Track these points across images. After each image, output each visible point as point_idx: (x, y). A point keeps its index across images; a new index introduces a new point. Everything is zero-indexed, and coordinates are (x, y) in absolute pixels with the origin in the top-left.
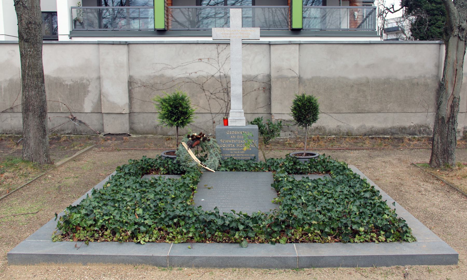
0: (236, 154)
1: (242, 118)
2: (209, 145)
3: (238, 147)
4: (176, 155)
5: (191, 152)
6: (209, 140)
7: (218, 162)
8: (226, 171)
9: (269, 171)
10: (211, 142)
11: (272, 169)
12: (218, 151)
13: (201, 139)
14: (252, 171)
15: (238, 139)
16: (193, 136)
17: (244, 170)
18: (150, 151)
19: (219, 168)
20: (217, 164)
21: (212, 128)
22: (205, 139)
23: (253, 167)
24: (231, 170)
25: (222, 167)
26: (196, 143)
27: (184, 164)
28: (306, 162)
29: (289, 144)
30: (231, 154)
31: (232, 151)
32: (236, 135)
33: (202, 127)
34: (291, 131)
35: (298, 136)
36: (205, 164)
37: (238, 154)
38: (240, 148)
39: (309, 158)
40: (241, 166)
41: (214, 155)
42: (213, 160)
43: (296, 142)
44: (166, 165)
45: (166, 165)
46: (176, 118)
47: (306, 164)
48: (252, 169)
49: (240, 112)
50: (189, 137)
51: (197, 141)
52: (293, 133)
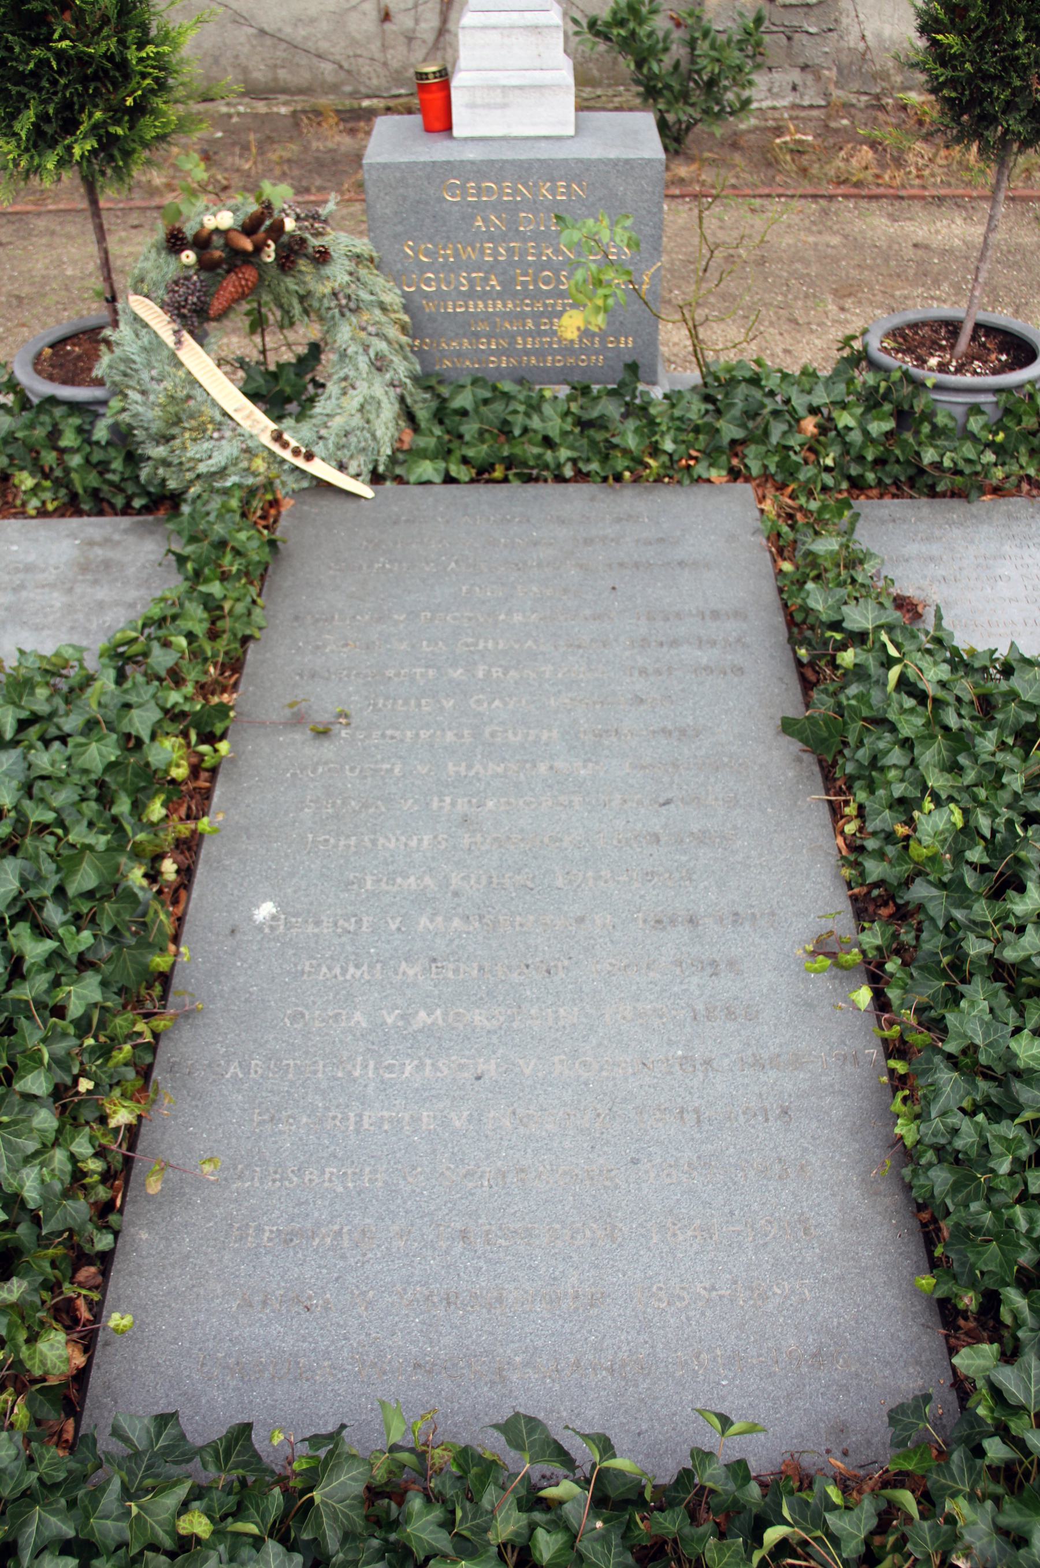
0: (512, 337)
1: (547, 77)
2: (326, 289)
3: (526, 294)
4: (99, 382)
5: (196, 359)
6: (323, 257)
7: (389, 410)
8: (449, 480)
9: (734, 475)
10: (338, 273)
11: (755, 471)
12: (393, 332)
13: (270, 254)
14: (618, 478)
15: (523, 238)
16: (202, 243)
17: (568, 472)
18: (41, 223)
19: (402, 456)
20: (386, 424)
21: (375, 47)
22: (292, 252)
23: (626, 452)
24: (482, 473)
25: (422, 454)
26: (231, 285)
27: (159, 451)
28: (975, 409)
29: (798, 151)
30: (477, 335)
31: (487, 317)
32: (513, 209)
33: (324, 46)
34: (804, 68)
35: (838, 94)
36: (306, 430)
37: (525, 334)
38: (537, 295)
39: (997, 391)
40: (548, 442)
41: (363, 362)
42: (362, 402)
43: (833, 140)
44: (49, 458)
45: (49, 458)
46: (44, 118)
47: (975, 424)
48: (620, 463)
49: (536, 29)
50: (175, 242)
51: (234, 275)
52: (810, 78)
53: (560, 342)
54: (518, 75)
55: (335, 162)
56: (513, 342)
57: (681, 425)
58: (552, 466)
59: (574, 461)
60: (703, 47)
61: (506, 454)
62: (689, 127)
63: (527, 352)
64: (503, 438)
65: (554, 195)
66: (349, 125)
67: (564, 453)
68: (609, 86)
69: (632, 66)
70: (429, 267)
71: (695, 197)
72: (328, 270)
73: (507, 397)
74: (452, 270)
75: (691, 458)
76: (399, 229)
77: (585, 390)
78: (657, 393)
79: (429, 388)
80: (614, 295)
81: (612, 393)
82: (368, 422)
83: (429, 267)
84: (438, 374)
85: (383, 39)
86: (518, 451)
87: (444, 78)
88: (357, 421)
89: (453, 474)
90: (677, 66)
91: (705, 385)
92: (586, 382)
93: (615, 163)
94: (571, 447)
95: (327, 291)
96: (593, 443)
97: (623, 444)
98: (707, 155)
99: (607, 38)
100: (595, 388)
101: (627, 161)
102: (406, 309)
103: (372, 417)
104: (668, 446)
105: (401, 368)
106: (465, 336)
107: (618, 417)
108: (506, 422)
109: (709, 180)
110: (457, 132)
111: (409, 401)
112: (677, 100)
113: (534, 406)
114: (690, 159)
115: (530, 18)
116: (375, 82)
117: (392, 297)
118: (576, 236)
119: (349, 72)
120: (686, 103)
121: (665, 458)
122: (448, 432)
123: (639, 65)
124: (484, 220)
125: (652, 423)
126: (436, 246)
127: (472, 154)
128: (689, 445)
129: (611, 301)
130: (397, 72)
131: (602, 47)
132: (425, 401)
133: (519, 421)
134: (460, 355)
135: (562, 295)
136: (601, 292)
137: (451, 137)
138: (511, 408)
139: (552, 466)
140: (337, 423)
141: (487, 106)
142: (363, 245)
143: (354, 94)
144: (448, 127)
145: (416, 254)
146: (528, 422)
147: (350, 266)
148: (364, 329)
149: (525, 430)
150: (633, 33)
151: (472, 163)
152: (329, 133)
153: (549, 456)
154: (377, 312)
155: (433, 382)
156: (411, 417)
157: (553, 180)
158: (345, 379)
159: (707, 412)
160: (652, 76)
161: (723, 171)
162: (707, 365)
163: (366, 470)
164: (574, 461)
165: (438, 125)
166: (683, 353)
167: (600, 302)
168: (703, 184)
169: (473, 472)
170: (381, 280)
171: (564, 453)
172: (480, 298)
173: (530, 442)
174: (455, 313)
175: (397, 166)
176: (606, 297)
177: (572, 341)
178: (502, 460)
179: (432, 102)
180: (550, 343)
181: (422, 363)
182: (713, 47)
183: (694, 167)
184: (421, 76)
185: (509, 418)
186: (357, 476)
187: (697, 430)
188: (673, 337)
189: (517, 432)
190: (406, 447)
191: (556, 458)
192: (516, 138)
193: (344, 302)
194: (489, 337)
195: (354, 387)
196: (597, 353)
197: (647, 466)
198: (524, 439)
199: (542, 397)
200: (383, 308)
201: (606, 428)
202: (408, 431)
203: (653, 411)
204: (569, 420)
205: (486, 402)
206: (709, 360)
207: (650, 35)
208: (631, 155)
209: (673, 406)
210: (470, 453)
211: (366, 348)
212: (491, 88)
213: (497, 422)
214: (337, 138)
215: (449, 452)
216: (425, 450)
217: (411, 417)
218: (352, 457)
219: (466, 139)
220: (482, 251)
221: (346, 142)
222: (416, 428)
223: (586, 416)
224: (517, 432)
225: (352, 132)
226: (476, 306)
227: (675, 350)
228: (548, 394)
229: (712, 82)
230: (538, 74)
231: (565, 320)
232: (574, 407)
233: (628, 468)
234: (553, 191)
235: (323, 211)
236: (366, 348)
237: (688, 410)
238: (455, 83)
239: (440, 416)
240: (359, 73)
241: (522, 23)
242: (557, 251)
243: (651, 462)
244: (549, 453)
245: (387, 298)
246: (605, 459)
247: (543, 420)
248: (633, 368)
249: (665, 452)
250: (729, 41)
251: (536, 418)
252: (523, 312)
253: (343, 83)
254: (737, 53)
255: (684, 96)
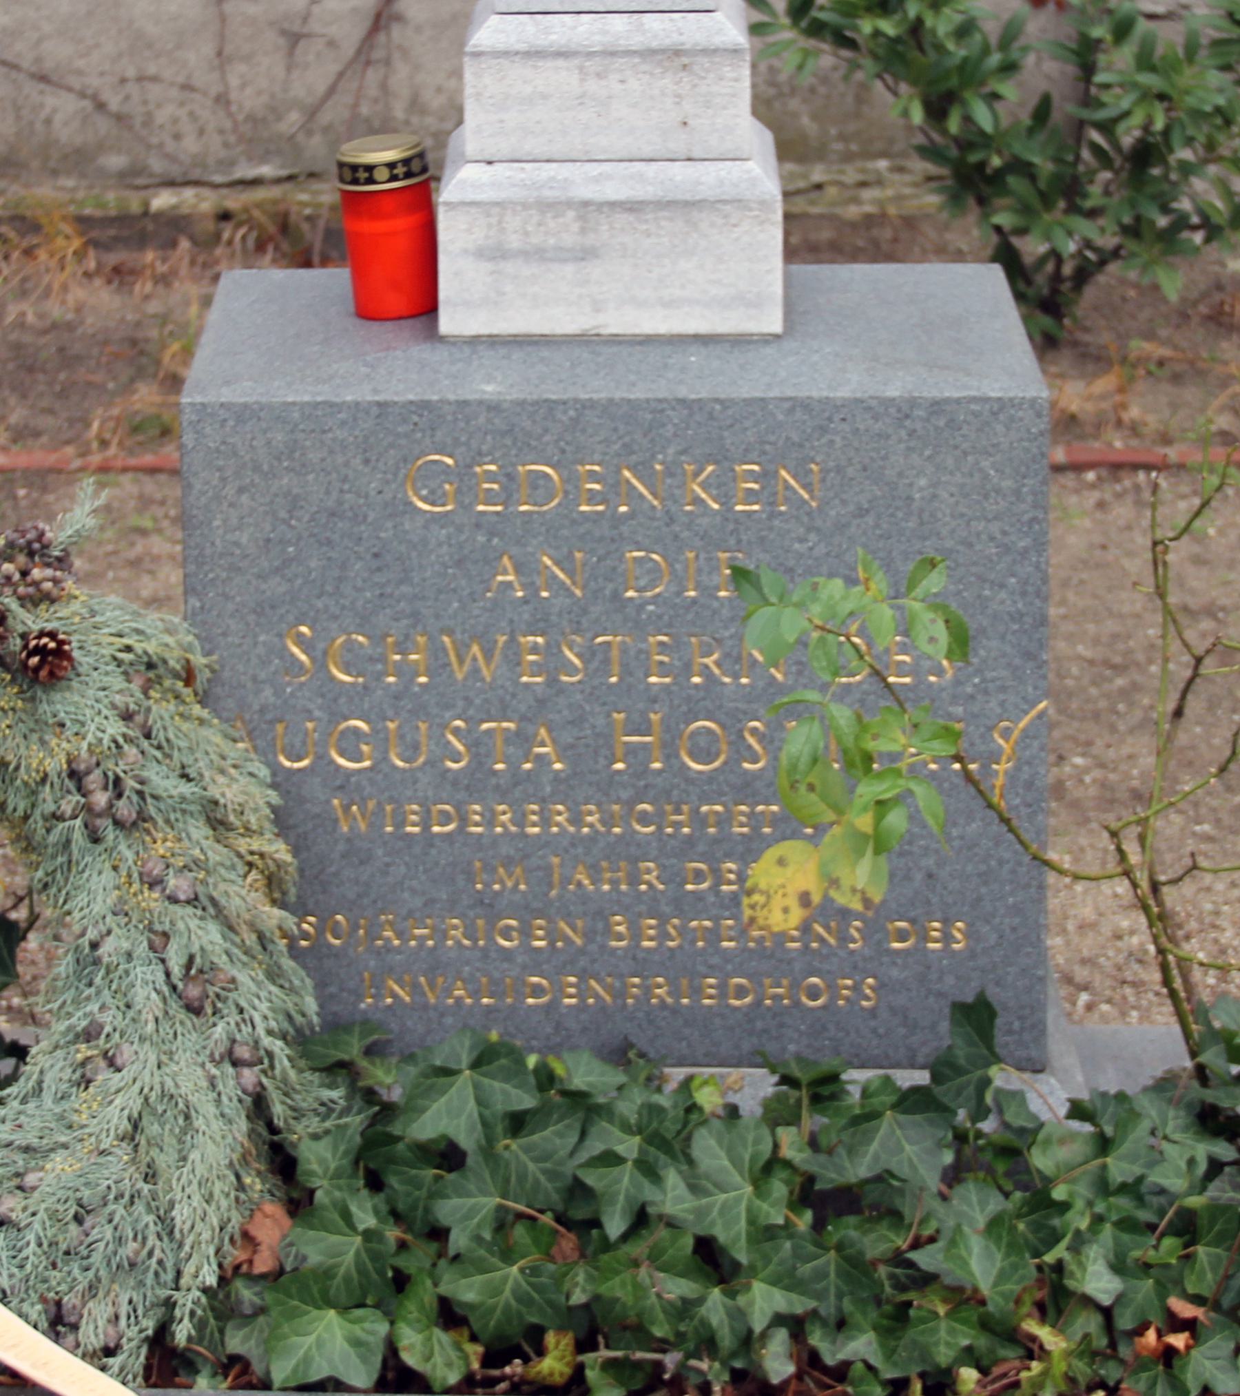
1: (707, 178)
7: (219, 1138)
10: (89, 711)
12: (243, 896)
15: (636, 622)
21: (197, 57)
23: (964, 1299)
30: (489, 907)
31: (523, 852)
33: (57, 52)
38: (676, 790)
40: (710, 1259)
41: (145, 985)
49: (675, 57)
53: (742, 932)
54: (622, 173)
55: (67, 359)
56: (598, 927)
57: (1139, 1213)
58: (726, 1341)
59: (796, 1326)
60: (1117, 63)
61: (578, 1298)
62: (1083, 275)
63: (641, 964)
64: (568, 1242)
65: (726, 500)
66: (112, 259)
67: (764, 1300)
68: (848, 157)
69: (917, 115)
70: (355, 700)
71: (1117, 468)
72: (60, 703)
73: (582, 1105)
74: (420, 711)
75: (1176, 1324)
76: (276, 587)
77: (824, 1091)
78: (1047, 1099)
79: (339, 1069)
80: (905, 797)
81: (914, 1102)
82: (150, 1176)
83: (355, 700)
84: (367, 1025)
85: (222, 37)
86: (617, 1288)
87: (418, 181)
88: (118, 1169)
89: (410, 1359)
90: (1042, 112)
91: (1201, 1074)
92: (828, 1063)
93: (904, 410)
94: (787, 1281)
95: (55, 764)
96: (856, 1267)
97: (951, 1273)
98: (1139, 346)
99: (844, 41)
100: (856, 1078)
101: (937, 406)
102: (282, 821)
103: (164, 1160)
104: (1097, 1280)
105: (261, 1005)
106: (452, 907)
107: (933, 1182)
108: (578, 1190)
109: (1153, 422)
110: (448, 322)
111: (278, 1110)
112: (1047, 201)
113: (668, 1140)
114: (1093, 360)
115: (658, 30)
116: (191, 145)
117: (244, 790)
118: (792, 624)
119: (121, 119)
120: (1073, 209)
121: (1090, 1323)
122: (396, 1216)
123: (937, 109)
124: (518, 569)
125: (1041, 1203)
126: (378, 639)
127: (489, 384)
128: (1169, 1281)
129: (896, 819)
130: (251, 118)
131: (827, 58)
132: (327, 1109)
133: (619, 1191)
134: (436, 965)
135: (747, 789)
136: (868, 790)
137: (432, 332)
138: (595, 1146)
139: (726, 1341)
140: (59, 1170)
141: (538, 254)
142: (166, 635)
143: (130, 177)
144: (425, 305)
145: (320, 664)
146: (649, 1192)
147: (125, 692)
148: (155, 883)
149: (641, 1219)
150: (916, 28)
151: (493, 408)
152: (59, 279)
153: (714, 1306)
154: (199, 830)
155: (353, 1049)
156: (282, 1162)
157: (722, 458)
158: (89, 1035)
159: (1215, 1167)
160: (975, 139)
161: (1191, 394)
162: (1202, 1013)
163: (134, 1336)
164: (796, 1326)
165: (395, 301)
166: (1111, 956)
167: (864, 823)
168: (1134, 430)
169: (475, 1351)
170: (213, 736)
171: (764, 1300)
172: (503, 794)
173: (656, 1258)
174: (428, 839)
175: (280, 414)
176: (881, 805)
177: (782, 937)
178: (569, 1317)
179: (381, 237)
180: (714, 936)
181: (320, 987)
182: (1145, 61)
183: (1105, 383)
184: (356, 172)
185: (590, 1178)
186: (103, 1355)
187: (1187, 1227)
188: (1089, 917)
189: (615, 1226)
190: (263, 1264)
191: (737, 1315)
192: (616, 340)
193: (101, 799)
194: (527, 912)
195: (112, 1064)
196: (857, 968)
197: (1032, 1350)
198: (638, 1248)
199: (693, 1108)
200: (218, 823)
201: (895, 1217)
202: (273, 1209)
203: (1041, 1160)
204: (779, 1188)
205: (518, 1123)
206: (1205, 996)
207: (964, 31)
208: (949, 388)
209: (1104, 1145)
210: (467, 1290)
211: (159, 940)
212: (547, 207)
213: (551, 1191)
214: (78, 293)
215: (401, 1282)
216: (327, 1274)
217: (282, 1162)
218: (92, 1290)
219: (474, 341)
220: (514, 658)
221: (101, 305)
222: (299, 1204)
223: (831, 1175)
224: (615, 1226)
225: (120, 275)
226: (490, 819)
227: (1087, 946)
228: (708, 1098)
229: (1145, 154)
230: (679, 171)
231: (764, 872)
232: (791, 1143)
233: (970, 1356)
234: (723, 488)
235: (58, 534)
236: (159, 940)
237: (1156, 1158)
238: (448, 194)
239: (372, 1166)
240: (148, 121)
241: (637, 42)
242: (735, 660)
243: (1044, 1334)
244: (716, 1293)
245: (229, 791)
246: (898, 1319)
247: (695, 1189)
248: (977, 1016)
249: (1088, 1301)
250: (1191, 50)
251: (672, 1177)
252: (629, 838)
253: (101, 147)
254: (1215, 78)
255: (1069, 190)
